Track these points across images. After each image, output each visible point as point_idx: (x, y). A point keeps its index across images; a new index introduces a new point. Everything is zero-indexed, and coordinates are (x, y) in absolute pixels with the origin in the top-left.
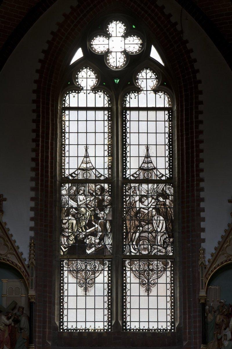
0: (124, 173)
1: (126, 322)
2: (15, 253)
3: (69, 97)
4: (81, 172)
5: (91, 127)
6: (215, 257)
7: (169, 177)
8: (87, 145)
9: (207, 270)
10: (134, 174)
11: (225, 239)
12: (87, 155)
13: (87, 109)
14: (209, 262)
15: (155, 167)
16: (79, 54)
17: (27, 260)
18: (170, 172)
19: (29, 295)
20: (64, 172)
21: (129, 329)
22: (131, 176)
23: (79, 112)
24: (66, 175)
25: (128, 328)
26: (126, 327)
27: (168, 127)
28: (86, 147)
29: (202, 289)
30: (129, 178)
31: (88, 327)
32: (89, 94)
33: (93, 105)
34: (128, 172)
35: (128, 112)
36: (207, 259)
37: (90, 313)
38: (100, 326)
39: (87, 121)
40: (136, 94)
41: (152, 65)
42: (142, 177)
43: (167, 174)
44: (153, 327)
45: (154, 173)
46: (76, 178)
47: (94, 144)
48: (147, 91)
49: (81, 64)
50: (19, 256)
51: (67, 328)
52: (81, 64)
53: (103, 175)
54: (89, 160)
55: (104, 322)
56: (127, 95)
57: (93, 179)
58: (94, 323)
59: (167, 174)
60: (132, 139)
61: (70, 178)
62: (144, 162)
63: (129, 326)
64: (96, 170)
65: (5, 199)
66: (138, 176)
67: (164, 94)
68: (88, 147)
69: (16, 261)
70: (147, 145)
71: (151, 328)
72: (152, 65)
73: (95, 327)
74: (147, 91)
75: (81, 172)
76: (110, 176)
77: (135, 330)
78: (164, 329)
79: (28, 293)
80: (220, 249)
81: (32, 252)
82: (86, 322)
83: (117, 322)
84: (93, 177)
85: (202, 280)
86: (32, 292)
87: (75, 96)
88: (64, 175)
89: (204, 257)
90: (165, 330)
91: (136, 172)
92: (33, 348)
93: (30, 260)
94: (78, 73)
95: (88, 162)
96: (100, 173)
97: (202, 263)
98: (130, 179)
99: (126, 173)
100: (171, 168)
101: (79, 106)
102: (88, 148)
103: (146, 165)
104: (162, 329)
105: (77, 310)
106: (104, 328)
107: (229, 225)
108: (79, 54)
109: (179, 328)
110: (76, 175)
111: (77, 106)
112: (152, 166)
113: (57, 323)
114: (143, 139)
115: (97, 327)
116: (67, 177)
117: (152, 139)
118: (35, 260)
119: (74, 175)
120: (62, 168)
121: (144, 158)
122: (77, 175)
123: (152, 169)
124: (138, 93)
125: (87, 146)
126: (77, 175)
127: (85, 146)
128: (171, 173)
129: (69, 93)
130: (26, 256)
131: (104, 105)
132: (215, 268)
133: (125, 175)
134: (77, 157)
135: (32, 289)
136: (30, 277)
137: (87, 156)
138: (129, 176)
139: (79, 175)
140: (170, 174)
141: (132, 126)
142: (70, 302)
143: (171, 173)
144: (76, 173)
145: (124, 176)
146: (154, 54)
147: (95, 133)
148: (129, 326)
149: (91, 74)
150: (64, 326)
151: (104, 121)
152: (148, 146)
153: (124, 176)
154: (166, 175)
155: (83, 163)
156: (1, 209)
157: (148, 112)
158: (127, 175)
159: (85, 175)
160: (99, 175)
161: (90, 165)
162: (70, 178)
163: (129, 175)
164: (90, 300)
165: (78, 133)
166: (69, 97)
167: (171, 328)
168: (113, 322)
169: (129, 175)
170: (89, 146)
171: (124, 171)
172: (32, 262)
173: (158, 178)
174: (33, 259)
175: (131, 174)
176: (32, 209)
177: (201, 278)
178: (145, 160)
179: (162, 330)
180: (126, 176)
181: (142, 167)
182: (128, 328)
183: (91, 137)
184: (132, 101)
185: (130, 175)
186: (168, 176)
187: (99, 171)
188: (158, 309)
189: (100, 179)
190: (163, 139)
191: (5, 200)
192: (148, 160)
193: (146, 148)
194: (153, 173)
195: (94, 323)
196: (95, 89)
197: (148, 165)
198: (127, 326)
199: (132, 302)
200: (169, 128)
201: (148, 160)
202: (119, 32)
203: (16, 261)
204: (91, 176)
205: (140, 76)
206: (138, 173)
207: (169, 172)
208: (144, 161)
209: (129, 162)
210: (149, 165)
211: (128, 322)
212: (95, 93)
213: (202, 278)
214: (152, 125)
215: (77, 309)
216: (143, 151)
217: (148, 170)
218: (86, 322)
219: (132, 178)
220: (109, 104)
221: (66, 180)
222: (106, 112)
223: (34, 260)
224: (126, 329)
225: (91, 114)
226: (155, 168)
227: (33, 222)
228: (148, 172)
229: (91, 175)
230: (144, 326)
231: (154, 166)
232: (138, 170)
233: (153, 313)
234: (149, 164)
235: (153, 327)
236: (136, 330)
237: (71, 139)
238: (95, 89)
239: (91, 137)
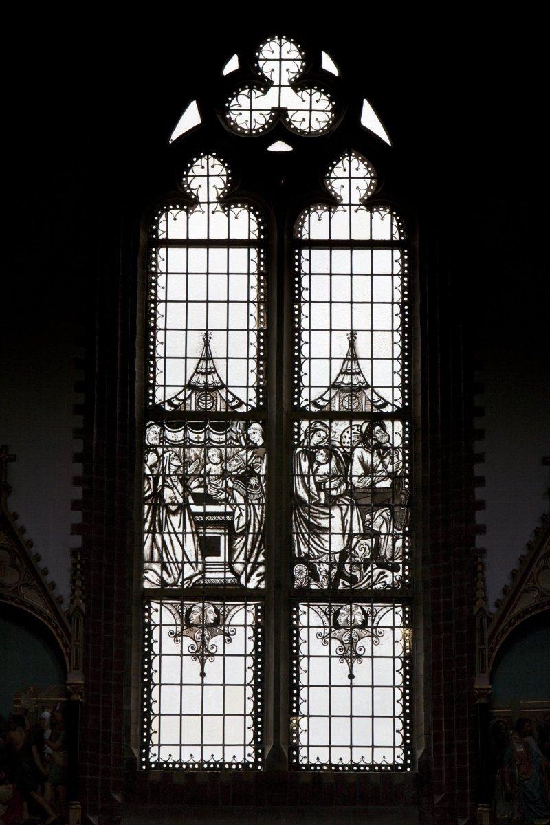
0: (296, 396)
1: (297, 748)
2: (35, 583)
3: (167, 219)
4: (193, 396)
5: (362, 289)
6: (511, 595)
7: (255, 406)
8: (207, 330)
9: (494, 623)
10: (172, 399)
11: (534, 548)
12: (207, 355)
13: (208, 243)
14: (497, 605)
15: (223, 383)
16: (191, 118)
17: (67, 601)
18: (403, 394)
19: (68, 682)
20: (154, 395)
21: (154, 763)
22: (166, 404)
23: (333, 251)
24: (156, 400)
25: (152, 760)
26: (148, 759)
27: (158, 287)
28: (207, 334)
29: (483, 672)
30: (308, 407)
31: (356, 760)
32: (213, 212)
33: (202, 235)
34: (305, 393)
35: (305, 253)
36: (491, 601)
37: (362, 726)
38: (388, 756)
39: (372, 275)
40: (183, 213)
41: (365, 145)
42: (336, 407)
43: (396, 400)
44: (318, 758)
45: (221, 396)
46: (327, 409)
47: (374, 329)
48: (350, 205)
49: (196, 144)
50: (45, 590)
51: (159, 758)
52: (196, 144)
53: (391, 402)
54: (212, 366)
55: (394, 747)
56: (160, 216)
57: (220, 412)
58: (392, 749)
59: (396, 400)
60: (314, 316)
61: (168, 408)
62: (199, 370)
63: (155, 755)
64: (373, 390)
65: (13, 457)
66: (326, 403)
67: (391, 213)
68: (210, 335)
69: (39, 604)
70: (207, 330)
71: (335, 761)
72: (365, 145)
73: (351, 761)
74: (350, 205)
75: (193, 396)
76: (407, 404)
77: (212, 766)
78: (217, 763)
79: (66, 678)
80: (522, 576)
81: (78, 583)
82: (202, 745)
83: (276, 747)
84: (367, 408)
85: (482, 650)
86: (76, 678)
87: (176, 217)
88: (153, 401)
89: (485, 598)
90: (220, 764)
91: (179, 394)
92: (78, 808)
93: (72, 602)
94: (195, 159)
95: (208, 370)
96: (382, 398)
97: (480, 610)
98: (308, 410)
99: (300, 396)
100: (407, 387)
101: (212, 237)
102: (210, 338)
103: (202, 379)
104: (212, 761)
105: (332, 718)
106: (394, 761)
107: (544, 518)
108: (191, 118)
109: (424, 763)
110: (326, 403)
111: (206, 238)
112: (362, 382)
113: (136, 752)
114: (197, 317)
115: (206, 759)
116: (160, 404)
117: (217, 317)
118: (84, 601)
119: (321, 403)
120: (149, 386)
121: (343, 360)
122: (330, 402)
123: (361, 389)
124: (187, 212)
125: (209, 332)
126: (184, 401)
127: (205, 332)
128: (261, 396)
129: (168, 210)
130: (63, 589)
131: (392, 236)
132: (510, 624)
133: (298, 400)
134: (188, 360)
135: (484, 673)
136: (73, 642)
137: (207, 357)
138: (308, 403)
139: (333, 402)
140: (404, 401)
141: (315, 288)
142: (165, 699)
143: (406, 397)
144: (181, 397)
145: (296, 403)
146: (370, 119)
147: (372, 303)
148: (155, 755)
149: (218, 167)
150: (300, 758)
151: (310, 274)
152: (209, 332)
153: (296, 403)
154: (396, 403)
155: (198, 373)
156: (3, 480)
157: (312, 251)
158: (401, 399)
159: (346, 404)
160: (234, 404)
161: (361, 378)
162: (168, 408)
163: (306, 400)
164: (213, 694)
165: (207, 302)
166: (167, 219)
167: (256, 759)
168: (268, 750)
169: (306, 400)
170: (213, 335)
171: (296, 390)
172: (78, 606)
173: (375, 411)
174: (81, 599)
175: (166, 399)
176: (77, 481)
177: (478, 647)
178: (200, 366)
179: (212, 763)
180: (299, 404)
181: (192, 384)
182: (152, 760)
183: (362, 312)
184: (316, 225)
185: (310, 402)
186: (399, 404)
187: (381, 391)
188: (202, 715)
189: (382, 412)
190: (387, 317)
191: (14, 459)
192: (207, 365)
193: (348, 338)
194: (218, 394)
195: (392, 749)
196: (371, 203)
197: (352, 379)
198: (150, 755)
199: (313, 701)
200: (259, 290)
201: (207, 365)
202: (288, 70)
203: (39, 604)
204: (216, 405)
205: (338, 171)
206: (327, 397)
207: (257, 396)
208: (197, 368)
209: (306, 374)
210: (210, 379)
211: (303, 746)
212: (371, 212)
213: (79, 643)
214: (361, 284)
215: (330, 716)
216: (196, 345)
217: (209, 389)
218: (351, 747)
219: (313, 409)
220: (401, 235)
221: (304, 414)
222: (397, 254)
223: (81, 601)
224: (148, 763)
225: (362, 255)
226: (367, 387)
227: (79, 513)
228: (351, 396)
229: (215, 403)
230: (340, 757)
231: (366, 381)
232: (182, 388)
233: (213, 724)
234: (354, 377)
235: (234, 757)
236: (215, 764)
237: (169, 316)
238: (371, 203)
239: (362, 312)
